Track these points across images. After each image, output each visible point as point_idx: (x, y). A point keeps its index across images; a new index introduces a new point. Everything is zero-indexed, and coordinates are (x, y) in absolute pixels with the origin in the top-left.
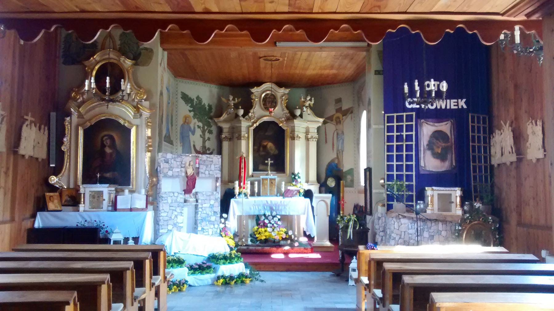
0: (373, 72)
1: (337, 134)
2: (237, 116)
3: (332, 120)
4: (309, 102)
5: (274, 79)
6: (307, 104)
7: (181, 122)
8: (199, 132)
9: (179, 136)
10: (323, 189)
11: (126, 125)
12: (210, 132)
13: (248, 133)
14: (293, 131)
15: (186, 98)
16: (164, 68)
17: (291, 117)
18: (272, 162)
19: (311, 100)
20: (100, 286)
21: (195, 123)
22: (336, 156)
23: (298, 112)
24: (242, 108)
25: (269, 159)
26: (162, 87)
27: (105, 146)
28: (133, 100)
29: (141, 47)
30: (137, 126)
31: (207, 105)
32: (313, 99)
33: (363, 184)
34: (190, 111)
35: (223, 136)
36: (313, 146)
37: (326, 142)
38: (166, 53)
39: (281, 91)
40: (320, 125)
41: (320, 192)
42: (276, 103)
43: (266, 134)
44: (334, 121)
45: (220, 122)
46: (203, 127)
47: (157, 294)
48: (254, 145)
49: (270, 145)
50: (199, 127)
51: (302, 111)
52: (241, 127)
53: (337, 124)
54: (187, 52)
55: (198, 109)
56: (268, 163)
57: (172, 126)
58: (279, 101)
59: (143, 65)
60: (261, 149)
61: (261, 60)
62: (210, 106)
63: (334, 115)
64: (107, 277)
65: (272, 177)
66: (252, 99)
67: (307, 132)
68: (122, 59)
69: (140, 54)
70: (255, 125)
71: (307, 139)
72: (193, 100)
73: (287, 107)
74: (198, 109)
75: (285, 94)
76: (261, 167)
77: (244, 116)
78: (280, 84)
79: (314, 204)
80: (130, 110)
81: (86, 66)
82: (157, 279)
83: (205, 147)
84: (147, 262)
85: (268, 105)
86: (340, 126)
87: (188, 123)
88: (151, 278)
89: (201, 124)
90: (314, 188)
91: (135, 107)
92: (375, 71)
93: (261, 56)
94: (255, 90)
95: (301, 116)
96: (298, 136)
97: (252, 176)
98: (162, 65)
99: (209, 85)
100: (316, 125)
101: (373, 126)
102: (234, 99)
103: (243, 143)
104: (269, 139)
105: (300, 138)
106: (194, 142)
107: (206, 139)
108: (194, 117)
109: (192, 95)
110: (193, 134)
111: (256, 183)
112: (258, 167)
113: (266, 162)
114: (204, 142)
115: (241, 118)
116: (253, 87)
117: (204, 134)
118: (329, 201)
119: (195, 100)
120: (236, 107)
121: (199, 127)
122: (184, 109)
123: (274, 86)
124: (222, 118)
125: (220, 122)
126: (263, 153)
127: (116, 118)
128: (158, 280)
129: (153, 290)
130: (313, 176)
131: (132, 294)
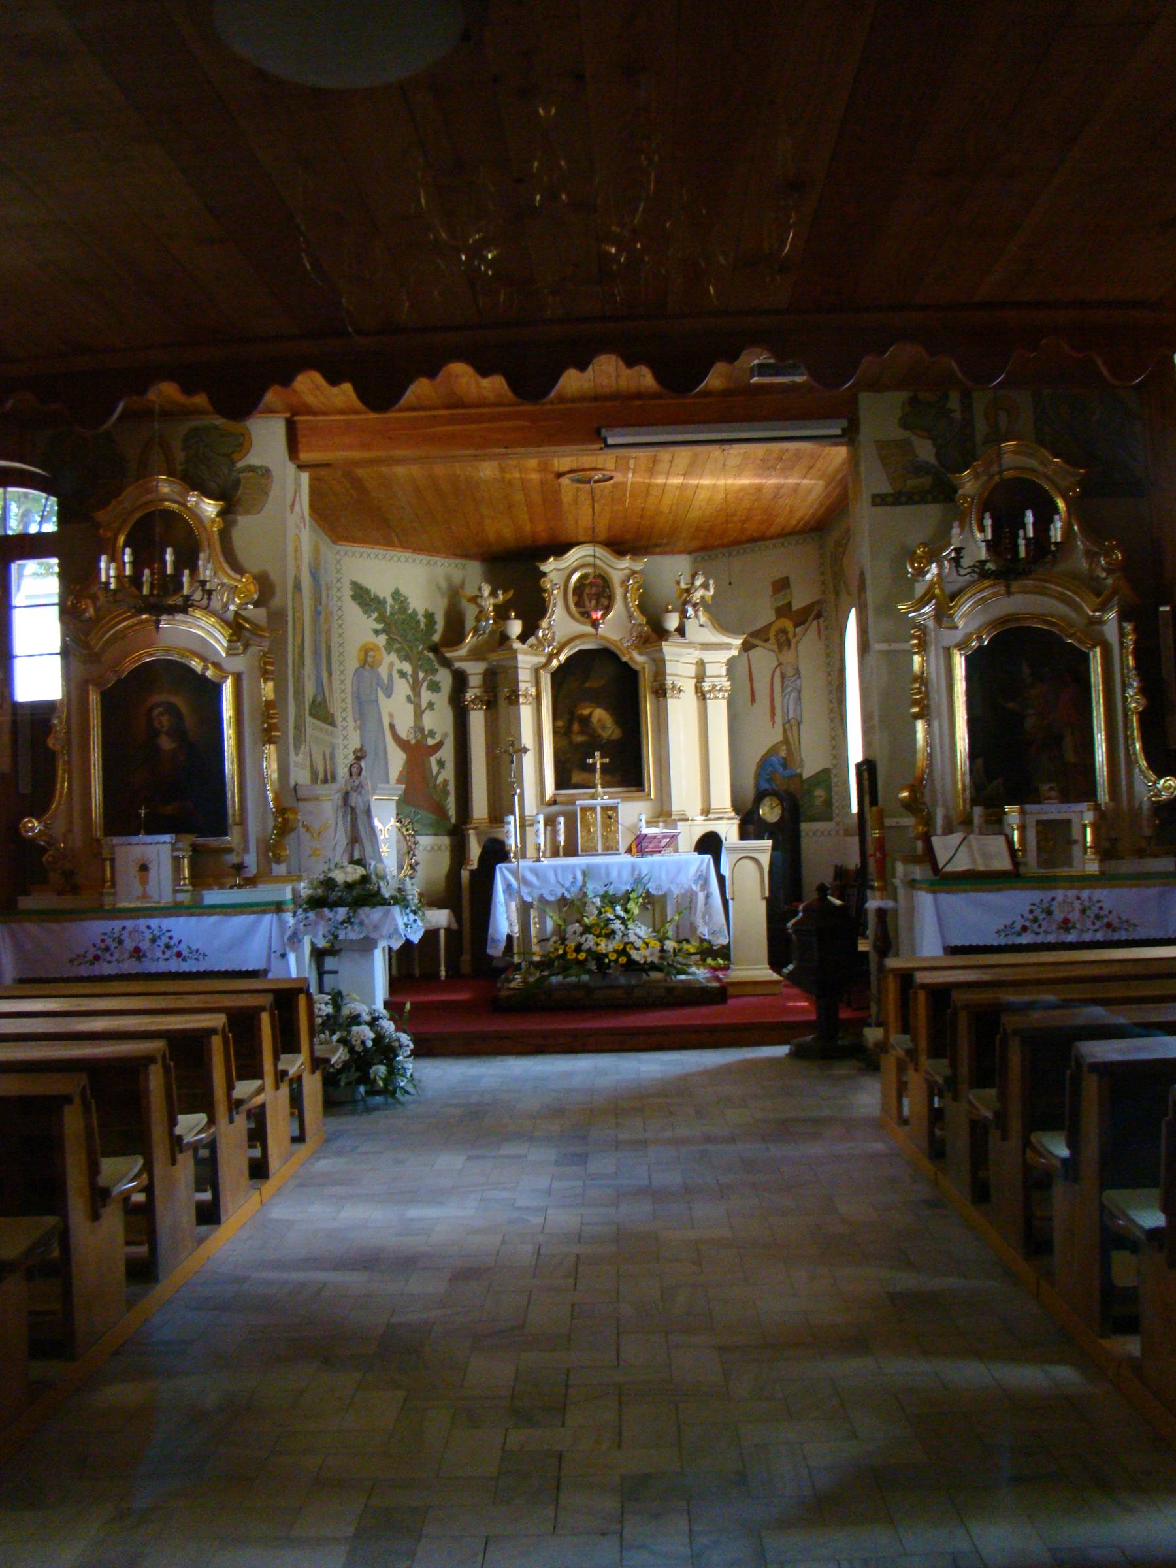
0: (866, 499)
1: (783, 676)
2: (504, 638)
3: (766, 640)
4: (701, 592)
5: (603, 536)
6: (697, 596)
7: (352, 664)
8: (402, 688)
9: (349, 700)
10: (751, 828)
11: (209, 673)
12: (434, 687)
13: (537, 685)
14: (659, 666)
15: (363, 596)
16: (303, 517)
17: (654, 636)
18: (607, 760)
19: (705, 586)
20: (146, 1067)
21: (391, 663)
22: (781, 738)
23: (672, 622)
24: (517, 617)
25: (597, 754)
26: (298, 568)
27: (157, 733)
28: (225, 606)
29: (240, 465)
30: (238, 679)
31: (421, 612)
32: (711, 582)
33: (855, 809)
34: (377, 632)
35: (470, 695)
36: (718, 710)
37: (753, 700)
38: (305, 477)
39: (620, 568)
40: (735, 653)
41: (743, 836)
42: (611, 599)
43: (587, 685)
44: (772, 640)
45: (461, 659)
46: (415, 675)
47: (296, 1100)
48: (555, 716)
49: (599, 715)
50: (402, 674)
51: (684, 615)
52: (517, 668)
53: (780, 649)
54: (360, 472)
55: (398, 625)
56: (595, 764)
57: (330, 674)
58: (619, 592)
59: (247, 512)
60: (576, 727)
61: (565, 481)
62: (430, 616)
63: (769, 626)
64: (159, 1045)
65: (606, 800)
66: (545, 591)
67: (700, 678)
68: (192, 499)
69: (237, 483)
70: (555, 663)
71: (701, 695)
72: (385, 601)
73: (642, 608)
74: (398, 625)
75: (635, 572)
76: (577, 777)
77: (523, 638)
78: (619, 546)
79: (725, 870)
80: (217, 635)
81: (98, 526)
82: (293, 1063)
83: (422, 730)
84: (265, 1017)
85: (587, 604)
86: (788, 656)
87: (372, 667)
88: (276, 1058)
89: (407, 667)
90: (728, 830)
91: (228, 624)
92: (874, 496)
93: (562, 469)
94: (550, 566)
95: (681, 631)
96: (674, 686)
97: (554, 802)
98: (297, 508)
99: (425, 558)
100: (724, 656)
101: (878, 647)
102: (493, 594)
103: (526, 712)
104: (597, 698)
105: (680, 691)
106: (391, 715)
107: (424, 706)
108: (389, 647)
109: (382, 588)
110: (389, 695)
111: (562, 820)
112: (570, 779)
113: (590, 761)
114: (418, 714)
115: (517, 645)
116: (545, 559)
117: (417, 694)
118: (765, 859)
119: (390, 601)
120: (502, 613)
121: (402, 674)
122: (359, 629)
123: (600, 552)
124: (463, 651)
125: (461, 659)
126: (579, 739)
127: (182, 656)
128: (295, 1064)
129: (285, 1090)
130: (722, 797)
131: (229, 1096)
